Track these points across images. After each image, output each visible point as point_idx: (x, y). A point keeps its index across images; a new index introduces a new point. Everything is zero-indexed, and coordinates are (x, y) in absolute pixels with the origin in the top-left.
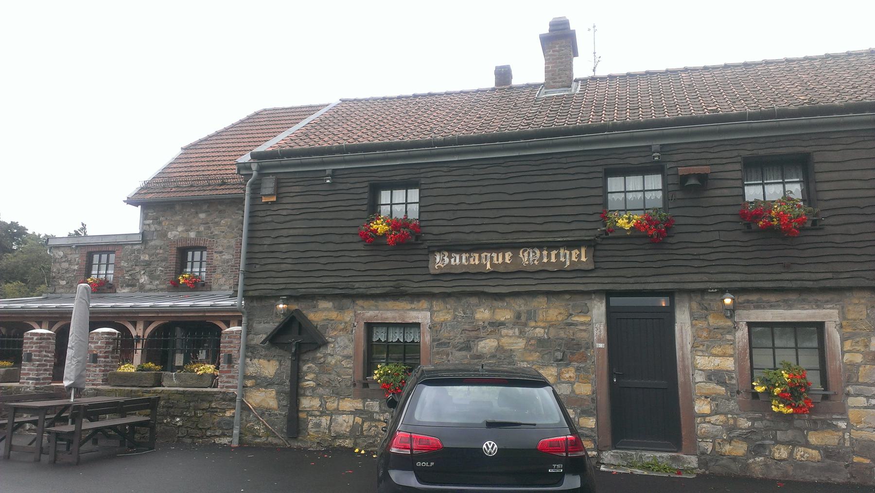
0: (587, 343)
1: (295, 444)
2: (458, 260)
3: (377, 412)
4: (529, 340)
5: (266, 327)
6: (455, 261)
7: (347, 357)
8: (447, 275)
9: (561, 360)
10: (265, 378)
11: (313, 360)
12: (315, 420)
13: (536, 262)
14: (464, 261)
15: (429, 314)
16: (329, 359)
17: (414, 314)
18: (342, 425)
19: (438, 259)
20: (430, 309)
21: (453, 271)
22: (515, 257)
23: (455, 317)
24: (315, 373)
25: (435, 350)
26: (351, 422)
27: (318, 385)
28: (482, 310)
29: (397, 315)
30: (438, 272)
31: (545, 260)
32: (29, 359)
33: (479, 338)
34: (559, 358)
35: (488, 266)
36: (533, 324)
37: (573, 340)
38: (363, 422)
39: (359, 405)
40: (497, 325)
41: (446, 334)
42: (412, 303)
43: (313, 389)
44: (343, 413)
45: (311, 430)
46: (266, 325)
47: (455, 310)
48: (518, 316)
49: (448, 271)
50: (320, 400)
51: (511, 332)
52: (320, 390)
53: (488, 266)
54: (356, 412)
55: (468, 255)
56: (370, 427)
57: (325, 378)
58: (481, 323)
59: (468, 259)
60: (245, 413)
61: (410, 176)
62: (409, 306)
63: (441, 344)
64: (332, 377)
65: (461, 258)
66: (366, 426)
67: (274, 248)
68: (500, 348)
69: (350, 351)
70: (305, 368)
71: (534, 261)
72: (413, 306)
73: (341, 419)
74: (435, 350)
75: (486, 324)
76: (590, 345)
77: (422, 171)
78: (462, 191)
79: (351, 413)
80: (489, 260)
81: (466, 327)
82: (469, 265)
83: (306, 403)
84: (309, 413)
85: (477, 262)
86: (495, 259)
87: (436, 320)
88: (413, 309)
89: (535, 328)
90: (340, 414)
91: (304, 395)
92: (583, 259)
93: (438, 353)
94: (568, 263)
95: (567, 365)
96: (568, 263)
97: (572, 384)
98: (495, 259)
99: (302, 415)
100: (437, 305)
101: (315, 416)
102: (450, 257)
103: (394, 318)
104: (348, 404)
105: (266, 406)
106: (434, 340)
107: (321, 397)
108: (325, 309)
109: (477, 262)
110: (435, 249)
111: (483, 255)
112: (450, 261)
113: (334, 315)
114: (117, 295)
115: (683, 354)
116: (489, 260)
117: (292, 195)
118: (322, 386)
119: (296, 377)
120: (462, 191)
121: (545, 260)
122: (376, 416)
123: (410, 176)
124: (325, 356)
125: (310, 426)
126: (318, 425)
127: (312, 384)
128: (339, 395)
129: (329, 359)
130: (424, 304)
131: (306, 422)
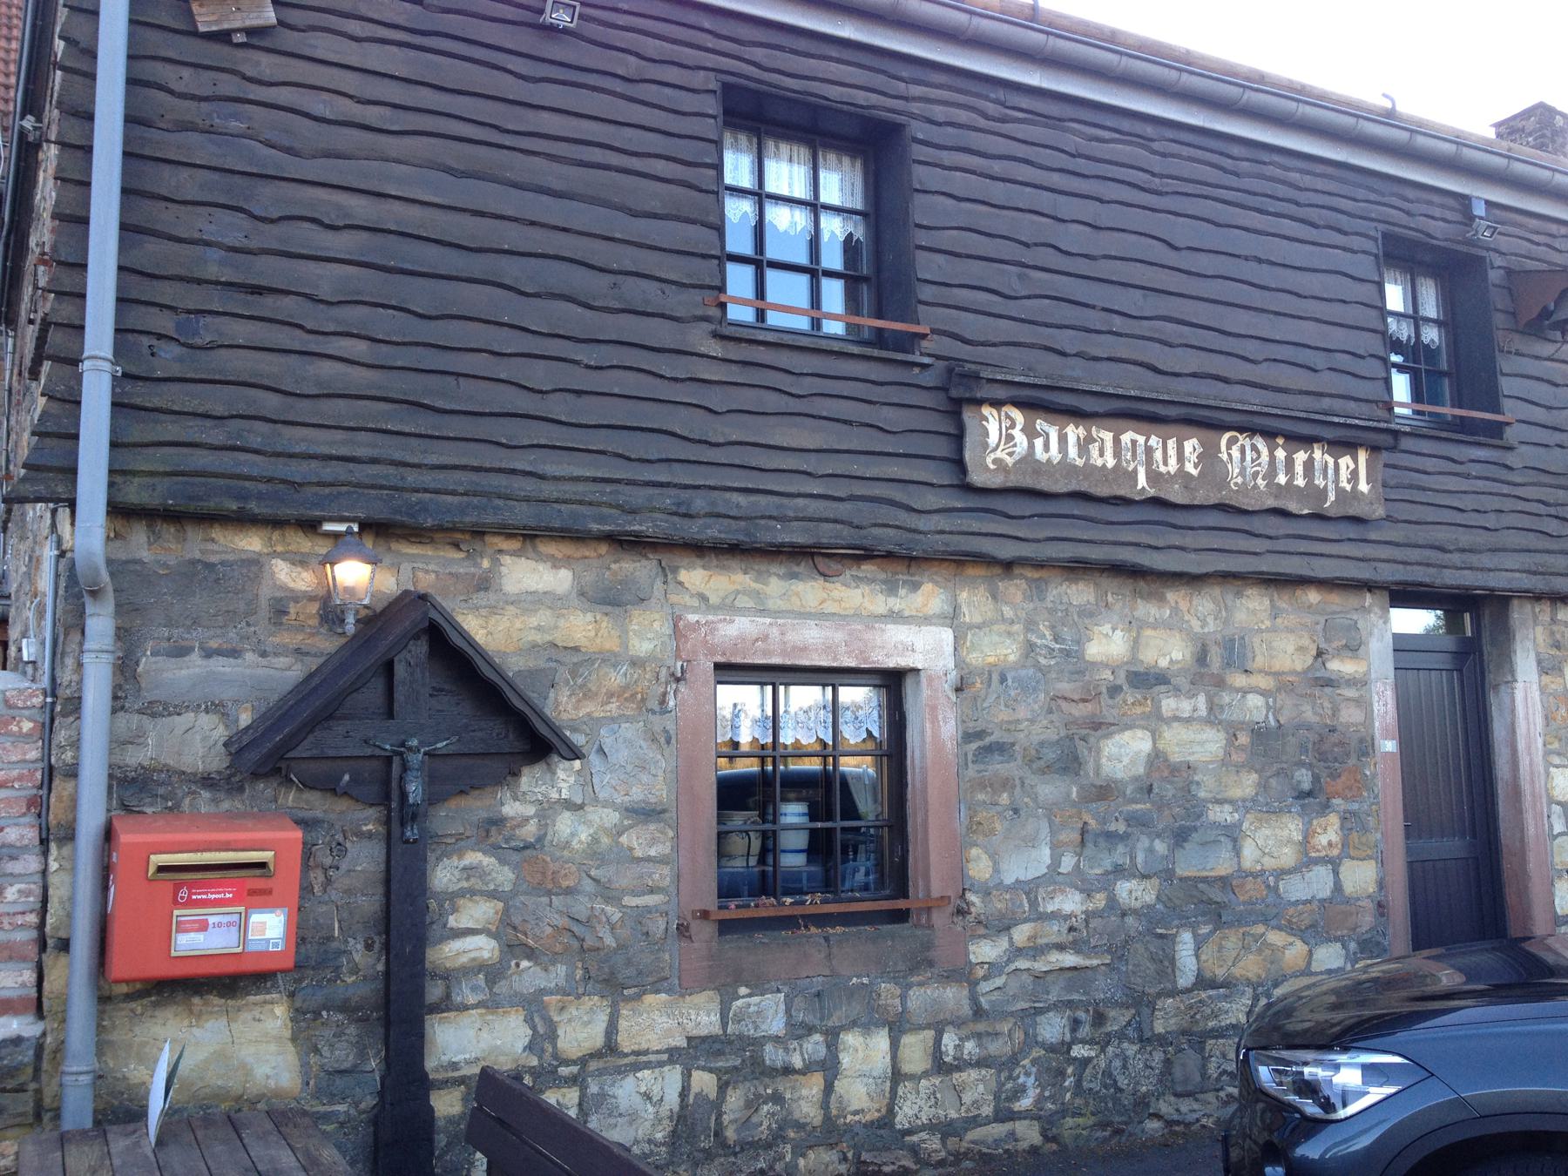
0: (1361, 741)
2: (1058, 446)
3: (776, 1039)
4: (1232, 730)
5: (224, 684)
6: (1047, 447)
7: (644, 813)
8: (1027, 494)
9: (1309, 794)
13: (1261, 482)
14: (1073, 451)
15: (947, 635)
16: (565, 824)
17: (898, 634)
18: (633, 1117)
19: (993, 427)
20: (952, 618)
21: (1044, 485)
22: (1209, 456)
23: (1030, 647)
24: (493, 895)
25: (971, 771)
26: (672, 1100)
28: (1107, 628)
29: (839, 636)
30: (997, 481)
31: (1282, 479)
33: (1098, 726)
34: (1306, 786)
35: (1142, 481)
36: (1240, 680)
37: (1333, 730)
38: (722, 1088)
39: (703, 1016)
40: (1147, 680)
41: (1004, 715)
42: (891, 589)
43: (493, 973)
44: (639, 1061)
46: (221, 665)
47: (1030, 625)
48: (1202, 658)
49: (1028, 482)
50: (529, 1020)
51: (1185, 707)
52: (528, 976)
53: (1142, 481)
54: (695, 1051)
55: (1081, 431)
56: (752, 1104)
57: (548, 917)
58: (1107, 675)
59: (1083, 447)
61: (874, 99)
62: (879, 603)
63: (989, 749)
64: (581, 907)
65: (1063, 439)
66: (734, 1100)
67: (267, 270)
68: (1157, 758)
69: (655, 787)
70: (444, 876)
71: (1255, 475)
72: (895, 603)
73: (626, 1091)
74: (971, 771)
75: (1121, 680)
76: (1366, 747)
77: (917, 90)
78: (1044, 200)
79: (673, 1055)
80: (1158, 459)
81: (1065, 687)
82: (1089, 469)
85: (1111, 462)
86: (1158, 455)
87: (974, 658)
88: (895, 617)
89: (1245, 692)
90: (621, 1071)
91: (446, 1005)
92: (1364, 487)
93: (982, 785)
94: (1332, 497)
95: (1325, 808)
96: (1332, 497)
97: (1334, 864)
98: (1158, 455)
100: (974, 600)
102: (1031, 433)
103: (828, 649)
104: (657, 1022)
106: (968, 737)
107: (532, 1006)
108: (536, 600)
109: (1111, 463)
110: (1000, 393)
111: (1126, 438)
112: (1031, 446)
113: (581, 627)
114: (1381, 227)
115: (1531, 764)
116: (1158, 459)
117: (354, 27)
118: (531, 954)
119: (404, 920)
120: (1044, 200)
121: (1282, 479)
122: (773, 1055)
123: (874, 99)
124: (547, 811)
127: (483, 948)
128: (614, 981)
129: (565, 824)
130: (930, 595)
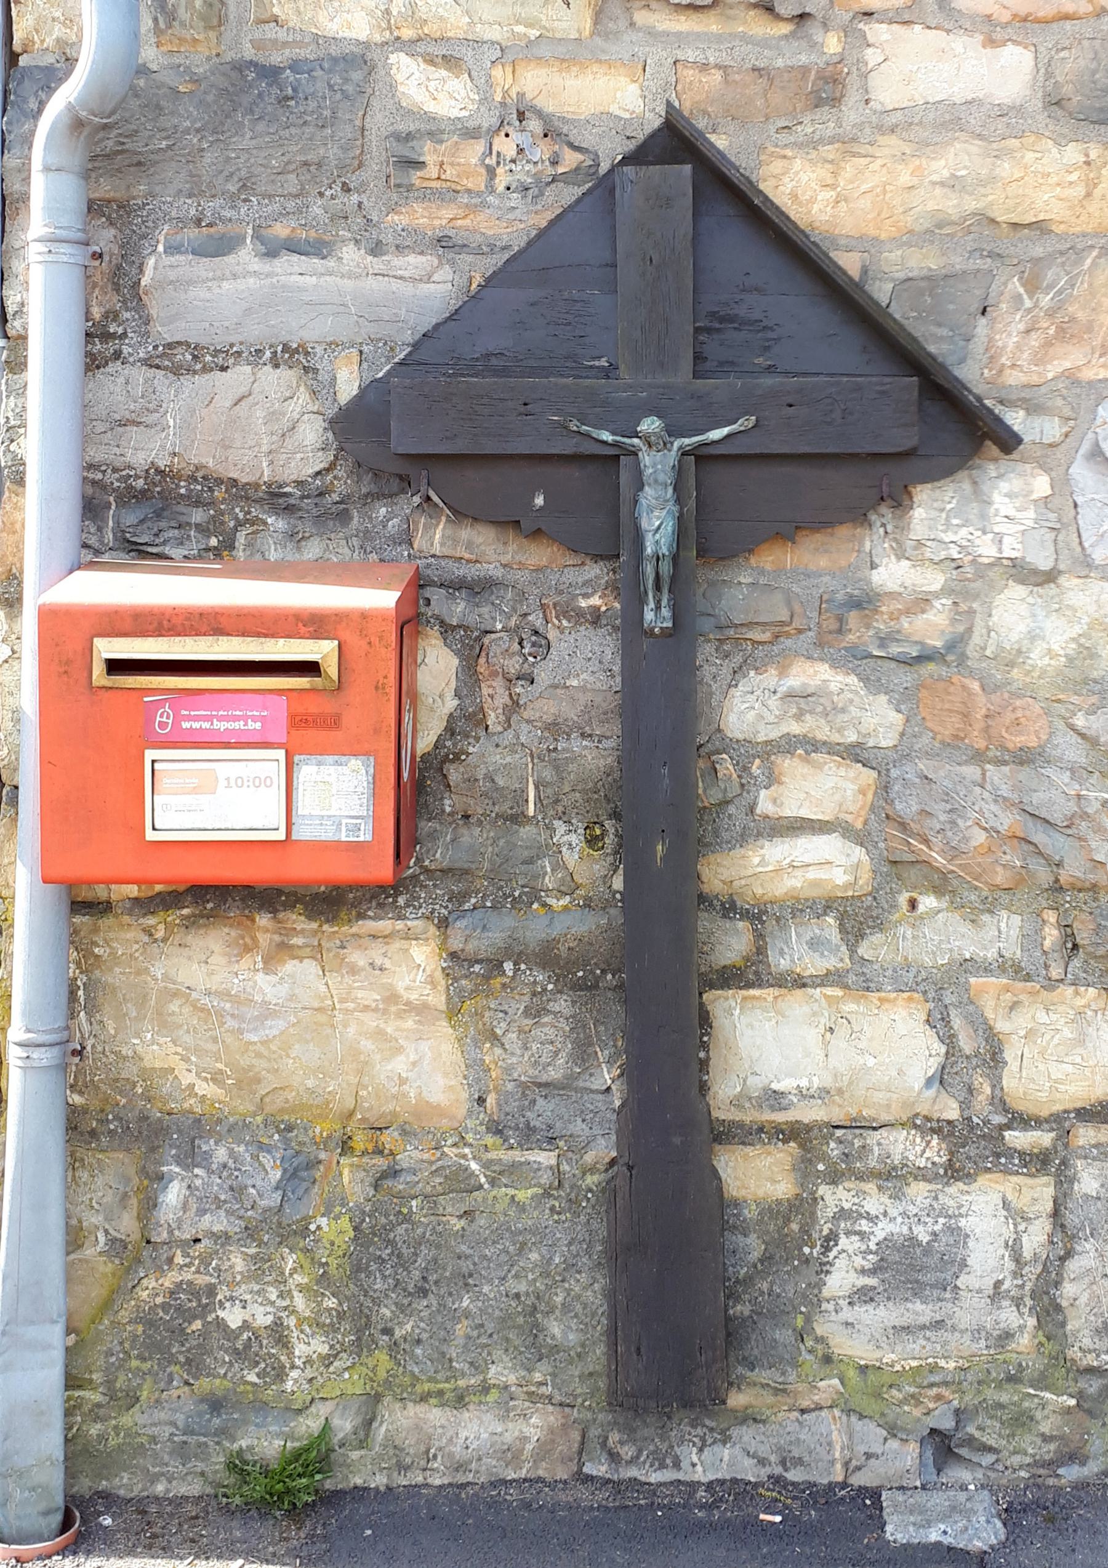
1: (707, 1462)
10: (779, 1202)
11: (845, 622)
12: (886, 1216)
27: (896, 868)
32: (1077, 993)
43: (857, 917)
45: (858, 1327)
52: (936, 933)
60: (113, 1170)
83: (773, 1047)
84: (822, 1145)
99: (755, 1176)
101: (893, 1177)
105: (339, 1089)
107: (942, 995)
108: (950, 120)
119: (664, 793)
125: (840, 1280)
126: (915, 1269)
129: (1011, 614)
131: (797, 1239)
